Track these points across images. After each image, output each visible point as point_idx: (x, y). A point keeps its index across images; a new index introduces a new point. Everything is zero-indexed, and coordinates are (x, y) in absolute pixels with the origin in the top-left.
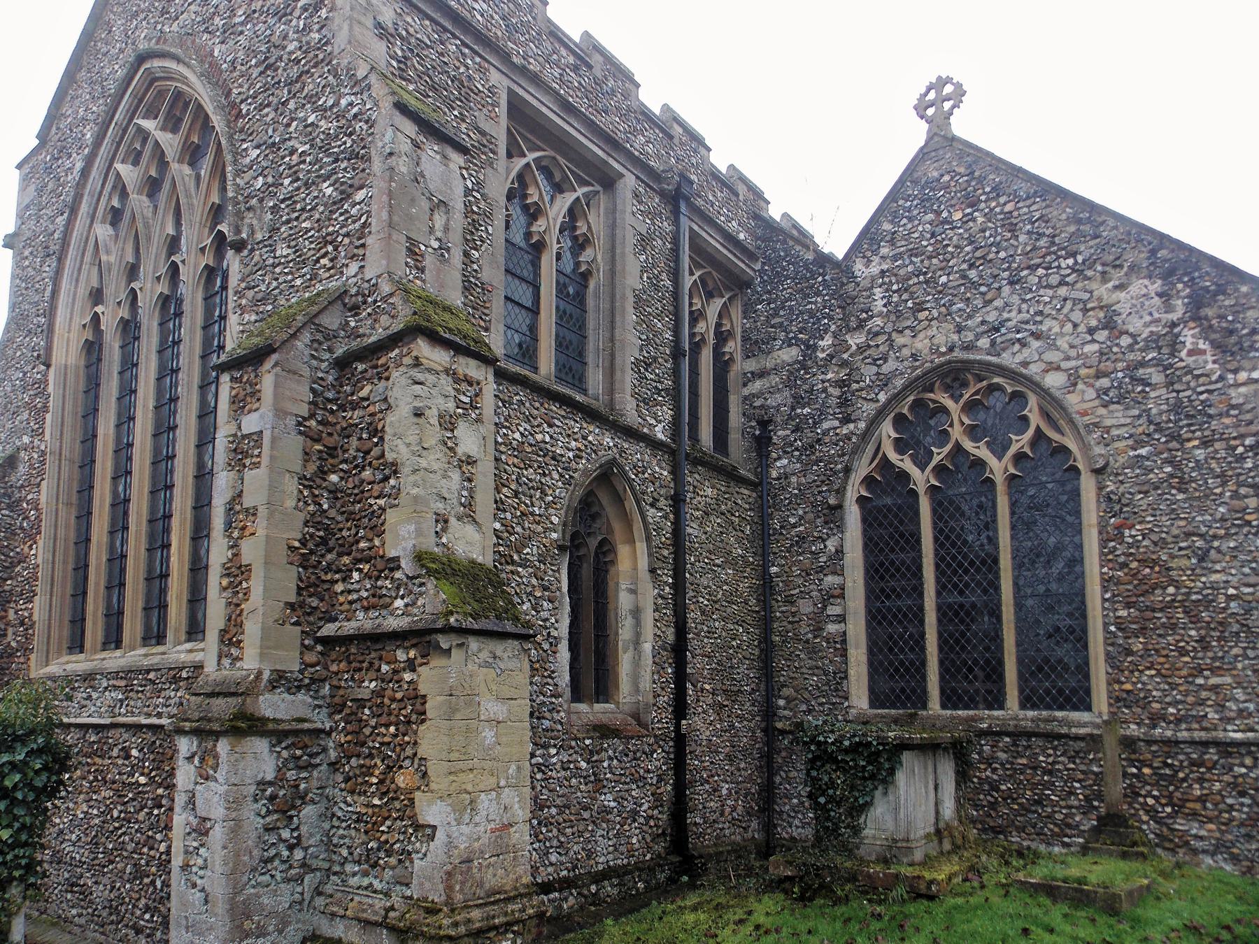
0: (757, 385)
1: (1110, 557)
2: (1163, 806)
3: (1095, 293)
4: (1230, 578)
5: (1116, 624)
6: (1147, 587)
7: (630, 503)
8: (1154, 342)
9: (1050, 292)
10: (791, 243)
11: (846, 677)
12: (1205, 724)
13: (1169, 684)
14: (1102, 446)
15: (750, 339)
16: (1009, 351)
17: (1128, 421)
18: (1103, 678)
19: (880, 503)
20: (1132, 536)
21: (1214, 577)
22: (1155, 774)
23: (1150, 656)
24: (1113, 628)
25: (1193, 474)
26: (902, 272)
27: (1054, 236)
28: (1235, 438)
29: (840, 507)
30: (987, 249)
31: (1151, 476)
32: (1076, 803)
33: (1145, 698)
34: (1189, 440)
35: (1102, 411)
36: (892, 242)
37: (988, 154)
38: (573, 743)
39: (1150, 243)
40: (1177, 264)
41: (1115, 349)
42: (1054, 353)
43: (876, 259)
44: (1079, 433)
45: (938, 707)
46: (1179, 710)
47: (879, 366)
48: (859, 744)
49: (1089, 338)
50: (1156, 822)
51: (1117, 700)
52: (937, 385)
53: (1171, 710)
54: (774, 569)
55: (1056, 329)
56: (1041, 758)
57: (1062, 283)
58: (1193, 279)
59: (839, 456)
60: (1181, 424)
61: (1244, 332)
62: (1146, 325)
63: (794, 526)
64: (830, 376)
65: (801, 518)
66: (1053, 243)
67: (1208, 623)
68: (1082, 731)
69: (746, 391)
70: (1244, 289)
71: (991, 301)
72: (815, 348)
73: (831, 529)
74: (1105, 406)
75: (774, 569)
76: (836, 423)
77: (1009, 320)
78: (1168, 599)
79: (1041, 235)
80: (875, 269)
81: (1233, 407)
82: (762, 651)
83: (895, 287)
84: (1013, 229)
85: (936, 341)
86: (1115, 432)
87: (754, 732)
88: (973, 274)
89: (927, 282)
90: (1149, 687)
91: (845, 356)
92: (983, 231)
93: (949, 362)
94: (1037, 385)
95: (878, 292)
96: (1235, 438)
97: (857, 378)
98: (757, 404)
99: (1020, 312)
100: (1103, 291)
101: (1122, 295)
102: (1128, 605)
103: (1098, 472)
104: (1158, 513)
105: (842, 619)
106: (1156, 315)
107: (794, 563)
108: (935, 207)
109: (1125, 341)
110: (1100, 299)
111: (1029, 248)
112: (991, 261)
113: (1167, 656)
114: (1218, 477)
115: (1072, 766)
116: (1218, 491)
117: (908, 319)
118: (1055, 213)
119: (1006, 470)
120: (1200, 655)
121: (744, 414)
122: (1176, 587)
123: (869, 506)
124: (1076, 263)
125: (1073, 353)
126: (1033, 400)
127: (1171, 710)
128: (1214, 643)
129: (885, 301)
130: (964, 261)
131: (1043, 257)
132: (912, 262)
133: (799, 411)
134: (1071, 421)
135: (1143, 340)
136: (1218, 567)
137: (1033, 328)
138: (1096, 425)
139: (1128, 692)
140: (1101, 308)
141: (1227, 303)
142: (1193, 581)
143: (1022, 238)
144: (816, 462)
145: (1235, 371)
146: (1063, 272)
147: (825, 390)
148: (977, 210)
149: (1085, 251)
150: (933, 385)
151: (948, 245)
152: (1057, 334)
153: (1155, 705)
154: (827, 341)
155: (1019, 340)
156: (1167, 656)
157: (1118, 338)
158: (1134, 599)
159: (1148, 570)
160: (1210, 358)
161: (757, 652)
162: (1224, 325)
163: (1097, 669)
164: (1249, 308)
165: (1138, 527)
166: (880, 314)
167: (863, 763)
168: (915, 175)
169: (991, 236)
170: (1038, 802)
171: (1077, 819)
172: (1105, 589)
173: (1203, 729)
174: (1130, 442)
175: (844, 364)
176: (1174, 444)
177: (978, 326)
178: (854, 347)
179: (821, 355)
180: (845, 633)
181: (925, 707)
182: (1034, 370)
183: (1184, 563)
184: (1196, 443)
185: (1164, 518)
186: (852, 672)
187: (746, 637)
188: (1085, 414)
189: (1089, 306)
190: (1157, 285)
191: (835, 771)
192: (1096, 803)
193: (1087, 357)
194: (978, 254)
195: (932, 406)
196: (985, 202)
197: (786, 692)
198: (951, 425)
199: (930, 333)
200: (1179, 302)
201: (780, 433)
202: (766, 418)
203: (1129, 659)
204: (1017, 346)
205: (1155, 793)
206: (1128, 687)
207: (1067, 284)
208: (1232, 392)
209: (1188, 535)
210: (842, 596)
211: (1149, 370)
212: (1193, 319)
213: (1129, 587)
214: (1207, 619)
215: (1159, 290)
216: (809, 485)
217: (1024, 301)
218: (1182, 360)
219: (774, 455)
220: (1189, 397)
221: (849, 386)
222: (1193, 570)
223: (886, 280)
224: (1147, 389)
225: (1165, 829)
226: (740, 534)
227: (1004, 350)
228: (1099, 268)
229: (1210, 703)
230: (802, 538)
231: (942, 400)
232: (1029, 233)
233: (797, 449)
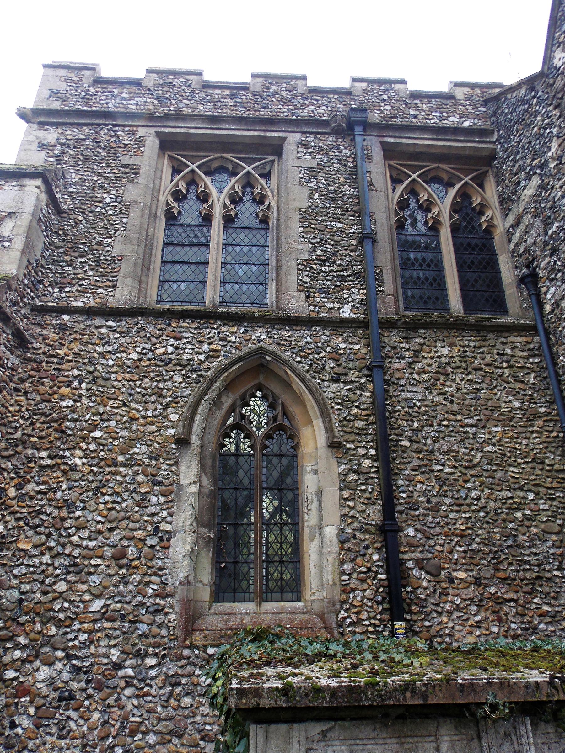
7: (298, 384)
38: (186, 652)
219: (544, 290)
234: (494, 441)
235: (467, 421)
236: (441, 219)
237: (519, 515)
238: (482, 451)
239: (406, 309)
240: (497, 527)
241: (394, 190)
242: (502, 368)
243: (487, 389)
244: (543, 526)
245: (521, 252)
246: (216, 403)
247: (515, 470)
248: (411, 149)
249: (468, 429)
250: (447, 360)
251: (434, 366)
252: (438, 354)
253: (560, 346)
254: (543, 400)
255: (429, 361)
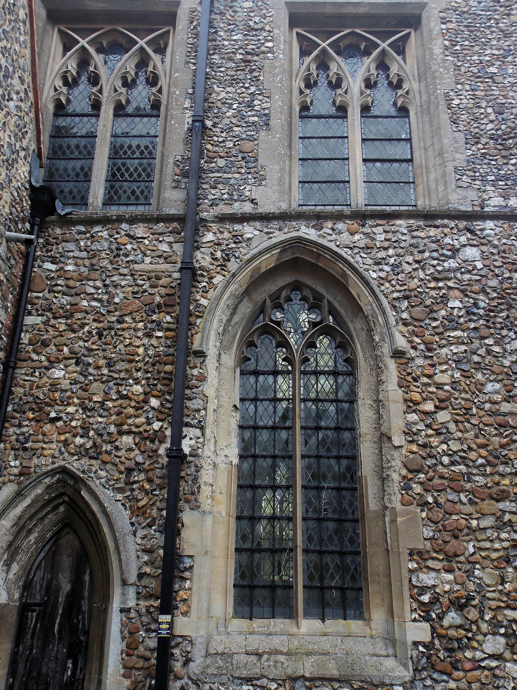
239: (108, 202)
241: (163, 62)
246: (239, 299)
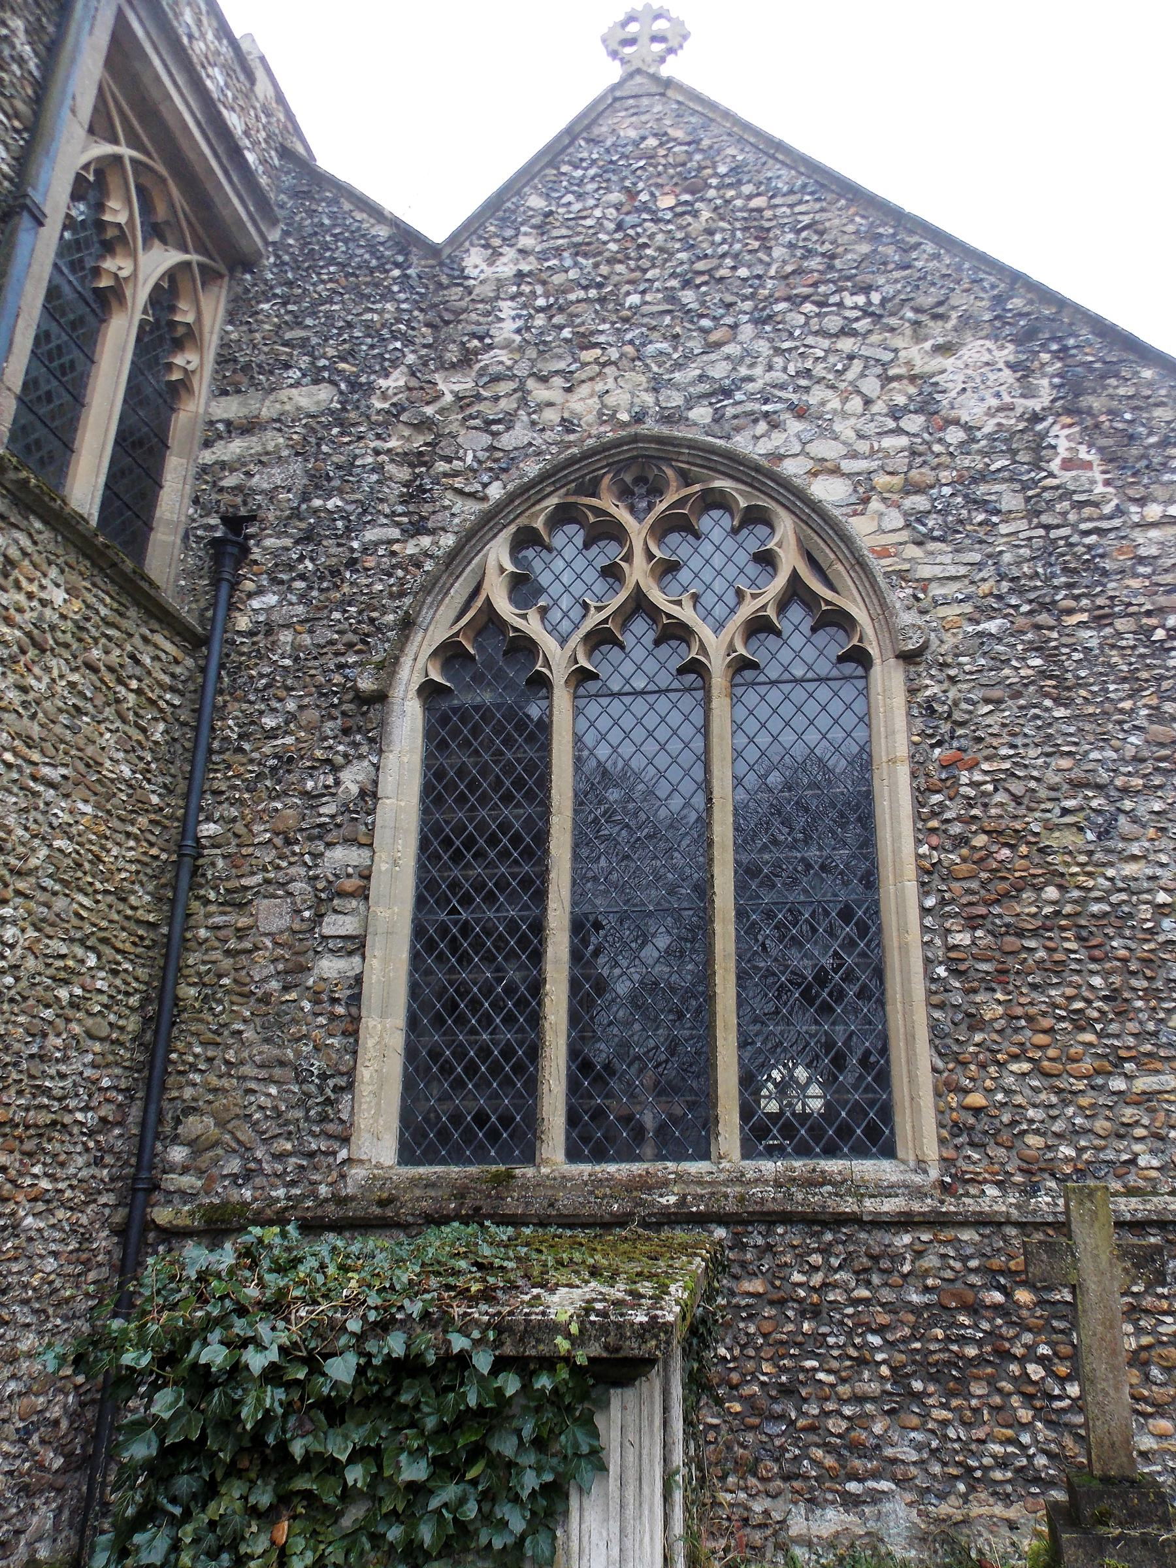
0: (235, 447)
1: (934, 823)
2: (1062, 1380)
3: (902, 354)
4: (1159, 872)
5: (948, 962)
6: (1004, 886)
8: (1003, 441)
9: (826, 343)
10: (347, 206)
11: (350, 1087)
12: (1133, 1180)
13: (1059, 1091)
14: (914, 612)
15: (235, 361)
16: (747, 434)
17: (963, 570)
18: (926, 1080)
19: (467, 699)
20: (973, 784)
21: (1130, 869)
22: (1041, 1303)
23: (1017, 1030)
24: (941, 971)
25: (1083, 673)
26: (558, 279)
27: (833, 257)
28: (1149, 614)
29: (381, 697)
30: (715, 262)
31: (1007, 671)
32: (874, 1388)
33: (1014, 1123)
34: (1070, 612)
35: (913, 551)
36: (542, 229)
37: (727, 114)
39: (993, 287)
40: (1040, 324)
41: (937, 448)
42: (831, 447)
43: (510, 253)
44: (873, 583)
45: (559, 1156)
46: (1081, 1150)
47: (495, 434)
48: (405, 1368)
49: (892, 424)
50: (1049, 1423)
51: (958, 1130)
52: (606, 481)
53: (1066, 1151)
54: (209, 829)
55: (835, 404)
56: (797, 1277)
57: (844, 332)
58: (1065, 349)
59: (392, 596)
60: (1056, 582)
61: (1153, 440)
62: (990, 413)
63: (272, 734)
64: (393, 443)
65: (291, 717)
66: (831, 267)
67: (1124, 960)
68: (890, 1206)
69: (207, 457)
70: (1147, 374)
71: (718, 345)
72: (369, 389)
73: (356, 745)
74: (919, 544)
75: (209, 829)
76: (395, 533)
77: (750, 379)
78: (1048, 910)
79: (809, 253)
80: (506, 267)
81: (1141, 560)
82: (147, 1021)
83: (541, 302)
84: (763, 235)
85: (610, 400)
86: (936, 590)
87: (86, 1238)
88: (688, 297)
89: (602, 300)
90: (1019, 1100)
91: (429, 410)
92: (710, 232)
93: (636, 438)
94: (801, 495)
95: (507, 308)
96: (1149, 614)
97: (448, 452)
98: (230, 481)
99: (770, 368)
100: (917, 356)
101: (949, 363)
102: (972, 923)
103: (908, 658)
104: (1019, 741)
105: (356, 945)
106: (1007, 399)
107: (259, 817)
108: (627, 183)
109: (954, 436)
110: (909, 364)
111: (789, 269)
112: (722, 279)
113: (1050, 1031)
114: (1124, 680)
115: (864, 1293)
116: (1127, 705)
117: (560, 357)
118: (837, 222)
119: (731, 648)
120: (1114, 1028)
121: (196, 501)
122: (1060, 887)
123: (444, 706)
124: (869, 303)
125: (863, 447)
126: (786, 525)
127: (1066, 1151)
128: (1139, 1004)
129: (520, 323)
130: (673, 275)
131: (815, 285)
132: (576, 264)
133: (317, 503)
134: (860, 564)
135: (985, 437)
136: (1135, 849)
137: (794, 398)
138: (902, 575)
139: (977, 1111)
140: (913, 379)
141: (1122, 391)
142: (1089, 874)
143: (778, 252)
144: (342, 605)
145: (1142, 502)
146: (848, 313)
147: (378, 468)
148: (702, 199)
149: (886, 286)
150: (596, 481)
151: (645, 245)
152: (835, 412)
153: (1033, 1140)
154: (397, 380)
155: (766, 415)
156: (1050, 1031)
157: (942, 429)
158: (982, 910)
159: (1006, 853)
160: (1100, 478)
161: (132, 1023)
162: (1120, 426)
163: (911, 1061)
164: (1157, 405)
165: (985, 766)
166: (507, 345)
167: (414, 1471)
168: (596, 131)
169: (724, 241)
170: (787, 1391)
171: (878, 1429)
172: (925, 889)
173: (1131, 1192)
174: (968, 608)
175: (424, 425)
176: (1043, 618)
177: (692, 383)
178: (449, 398)
179: (379, 405)
180: (359, 980)
181: (530, 1157)
182: (792, 468)
183: (1069, 839)
184: (1084, 617)
185: (1033, 752)
186: (365, 1074)
187: (104, 984)
188: (884, 553)
189: (891, 373)
190: (1008, 352)
191: (267, 1517)
192: (917, 1385)
193: (888, 456)
194: (700, 266)
195: (592, 519)
196: (718, 188)
197: (194, 1126)
198: (628, 558)
199: (599, 387)
200: (1045, 382)
201: (269, 542)
202: (243, 512)
203: (978, 1038)
204: (762, 427)
205: (1044, 1350)
206: (977, 1099)
207: (854, 333)
208: (1139, 536)
209: (1077, 785)
210: (363, 894)
211: (997, 488)
212: (1068, 412)
213: (975, 885)
214: (1122, 953)
215: (1011, 358)
216: (319, 651)
217: (778, 351)
218: (1051, 475)
219: (249, 586)
220: (1066, 538)
221: (429, 465)
222: (1090, 853)
223: (526, 289)
224: (995, 519)
225: (1068, 1441)
226: (137, 735)
227: (738, 429)
228: (910, 315)
229: (1140, 1132)
230: (287, 761)
231: (613, 510)
232: (791, 246)
233: (302, 577)
234: (74, 830)
235: (46, 771)
236: (128, 293)
237: (63, 993)
238: (50, 846)
240: (23, 1012)
242: (126, 686)
243: (93, 718)
244: (90, 1022)
245: (224, 483)
247: (86, 902)
248: (156, 94)
249: (41, 788)
250: (55, 618)
251: (28, 615)
252: (44, 595)
253: (236, 700)
254: (160, 780)
255: (21, 598)
